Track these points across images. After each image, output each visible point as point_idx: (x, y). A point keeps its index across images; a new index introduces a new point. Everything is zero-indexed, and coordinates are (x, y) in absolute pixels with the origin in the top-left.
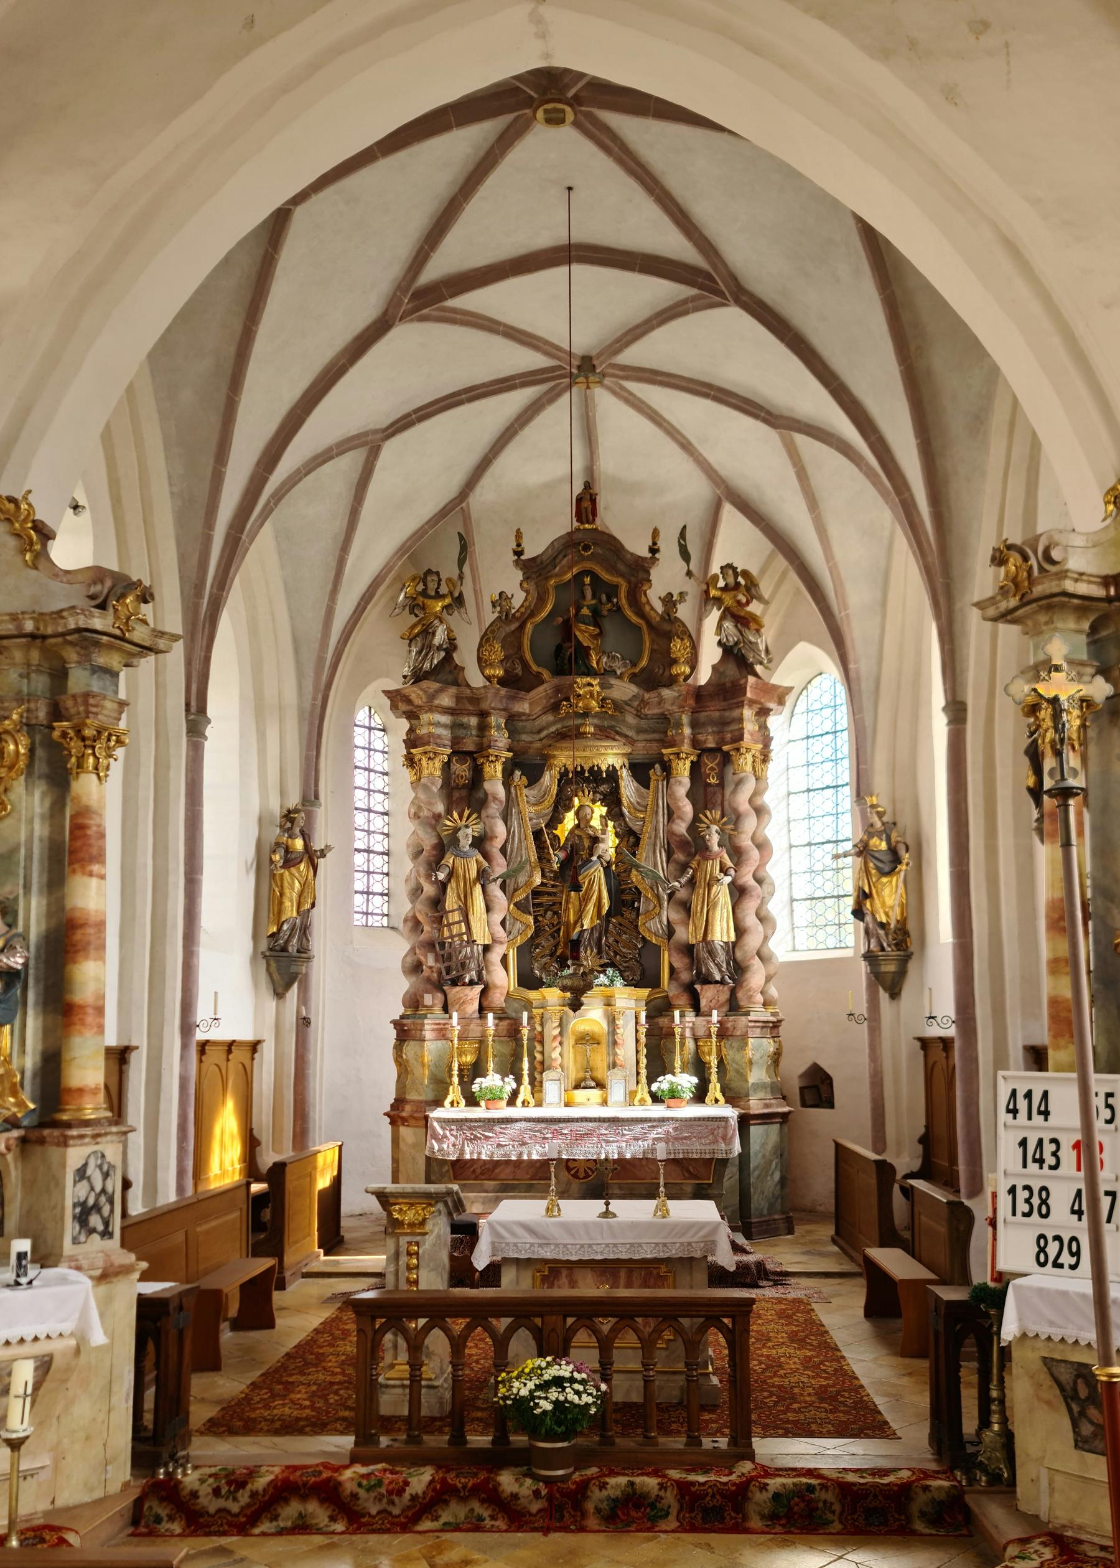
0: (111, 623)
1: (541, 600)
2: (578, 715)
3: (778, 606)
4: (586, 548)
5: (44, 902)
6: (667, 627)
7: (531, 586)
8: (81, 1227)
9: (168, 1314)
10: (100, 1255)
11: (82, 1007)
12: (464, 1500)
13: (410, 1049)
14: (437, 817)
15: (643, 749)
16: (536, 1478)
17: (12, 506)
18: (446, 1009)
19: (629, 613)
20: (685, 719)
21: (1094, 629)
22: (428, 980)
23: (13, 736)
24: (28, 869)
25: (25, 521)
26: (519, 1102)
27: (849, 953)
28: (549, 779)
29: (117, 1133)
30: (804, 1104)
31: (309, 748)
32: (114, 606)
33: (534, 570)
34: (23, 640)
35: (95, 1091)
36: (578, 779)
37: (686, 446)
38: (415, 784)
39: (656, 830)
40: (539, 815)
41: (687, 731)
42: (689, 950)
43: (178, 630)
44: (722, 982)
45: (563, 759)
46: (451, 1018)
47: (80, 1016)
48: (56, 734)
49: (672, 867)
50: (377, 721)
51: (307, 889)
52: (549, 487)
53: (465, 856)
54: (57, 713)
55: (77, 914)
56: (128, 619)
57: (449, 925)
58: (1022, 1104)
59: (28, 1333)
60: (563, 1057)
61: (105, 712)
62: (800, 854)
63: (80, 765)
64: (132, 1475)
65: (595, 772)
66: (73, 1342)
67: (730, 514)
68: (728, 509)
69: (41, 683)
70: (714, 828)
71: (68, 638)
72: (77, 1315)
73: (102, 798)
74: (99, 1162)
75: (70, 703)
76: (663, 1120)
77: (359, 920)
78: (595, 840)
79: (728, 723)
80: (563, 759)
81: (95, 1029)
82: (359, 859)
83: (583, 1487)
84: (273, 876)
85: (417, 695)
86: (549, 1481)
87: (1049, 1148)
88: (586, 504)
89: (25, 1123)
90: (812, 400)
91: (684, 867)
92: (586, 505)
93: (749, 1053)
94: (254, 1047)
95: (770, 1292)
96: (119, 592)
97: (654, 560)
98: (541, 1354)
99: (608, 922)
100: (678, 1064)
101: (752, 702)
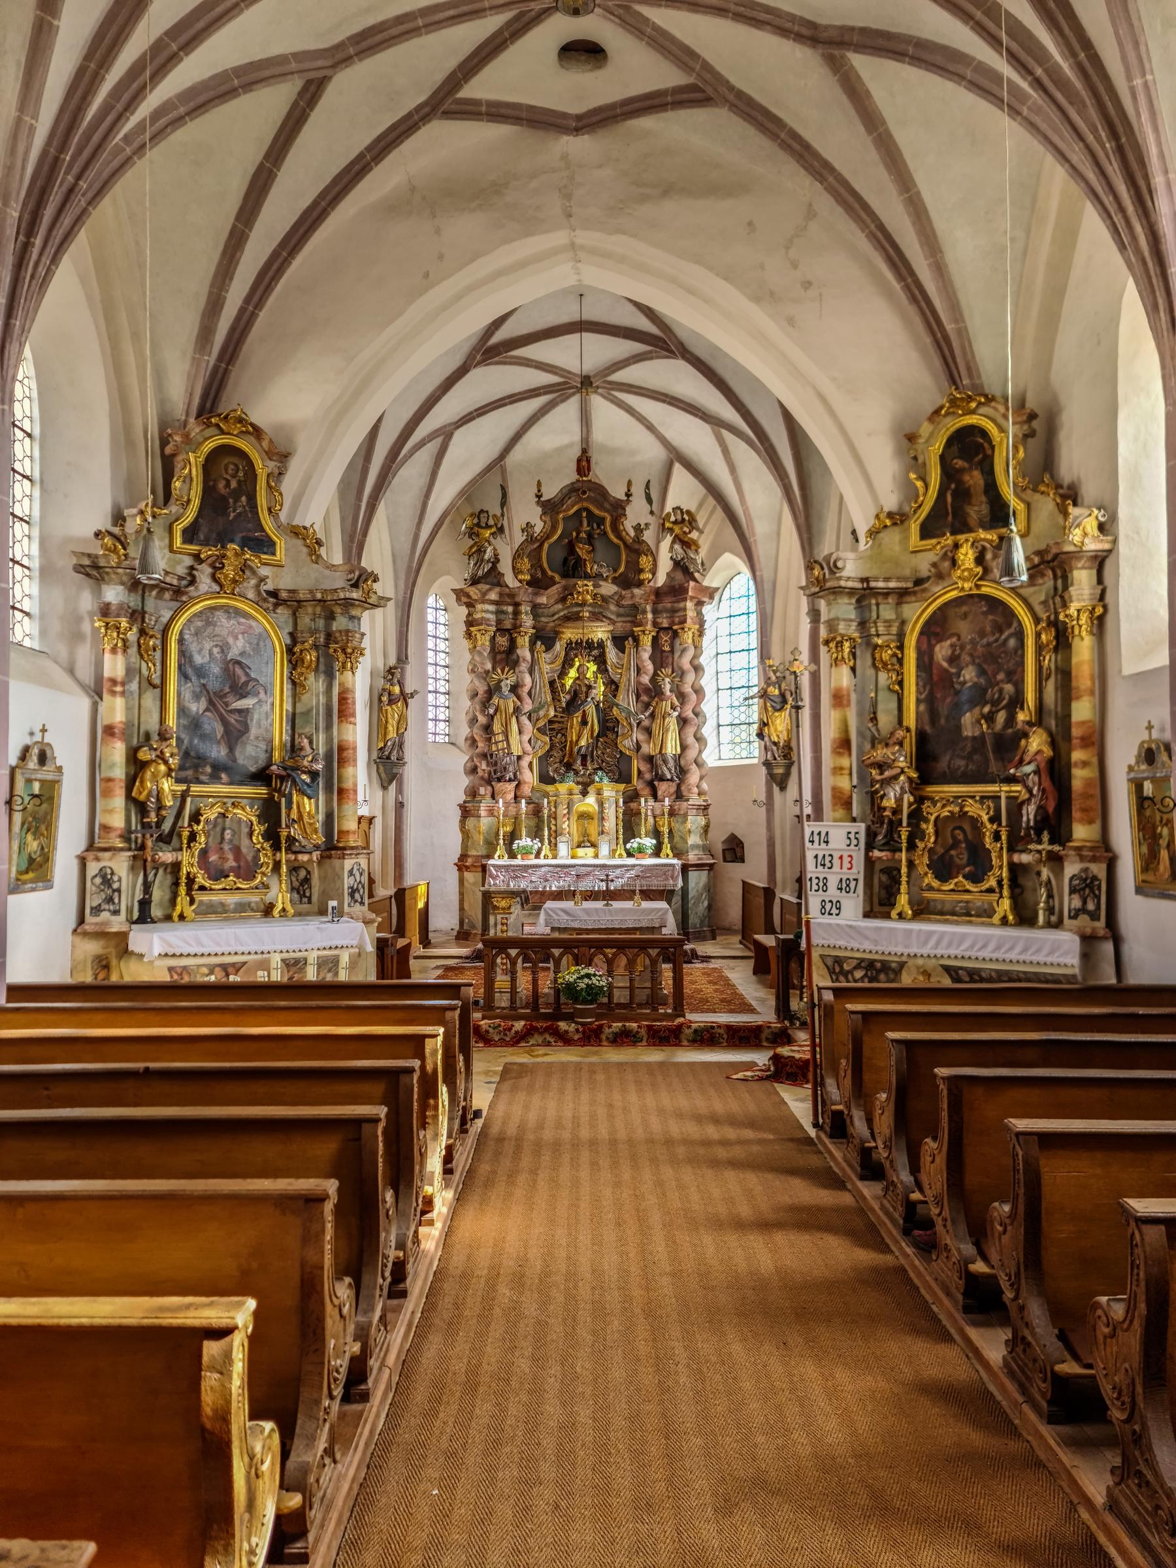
1: (554, 528)
2: (577, 605)
3: (711, 529)
4: (584, 493)
6: (637, 546)
7: (548, 519)
12: (541, 1033)
13: (470, 822)
14: (487, 672)
15: (621, 627)
16: (577, 1023)
18: (493, 797)
19: (612, 537)
20: (649, 608)
21: (858, 601)
22: (482, 778)
26: (542, 855)
27: (755, 761)
28: (559, 647)
30: (725, 860)
31: (401, 626)
33: (549, 508)
36: (574, 648)
37: (650, 428)
38: (473, 650)
39: (629, 680)
40: (553, 671)
41: (650, 616)
42: (650, 759)
43: (392, 596)
44: (672, 780)
45: (570, 634)
46: (497, 802)
48: (331, 650)
49: (639, 705)
50: (441, 603)
51: (402, 719)
52: (559, 450)
53: (506, 698)
57: (496, 743)
58: (816, 838)
60: (569, 826)
62: (724, 695)
65: (590, 645)
67: (678, 470)
68: (677, 467)
69: (321, 623)
70: (667, 680)
76: (634, 866)
77: (431, 738)
78: (589, 687)
79: (677, 611)
80: (570, 634)
82: (431, 697)
83: (601, 1027)
84: (380, 709)
85: (474, 592)
86: (583, 1024)
87: (828, 859)
88: (584, 463)
90: (729, 413)
91: (647, 706)
92: (584, 464)
93: (689, 825)
94: (371, 820)
95: (698, 965)
97: (628, 501)
98: (577, 965)
99: (598, 741)
100: (643, 831)
101: (692, 598)
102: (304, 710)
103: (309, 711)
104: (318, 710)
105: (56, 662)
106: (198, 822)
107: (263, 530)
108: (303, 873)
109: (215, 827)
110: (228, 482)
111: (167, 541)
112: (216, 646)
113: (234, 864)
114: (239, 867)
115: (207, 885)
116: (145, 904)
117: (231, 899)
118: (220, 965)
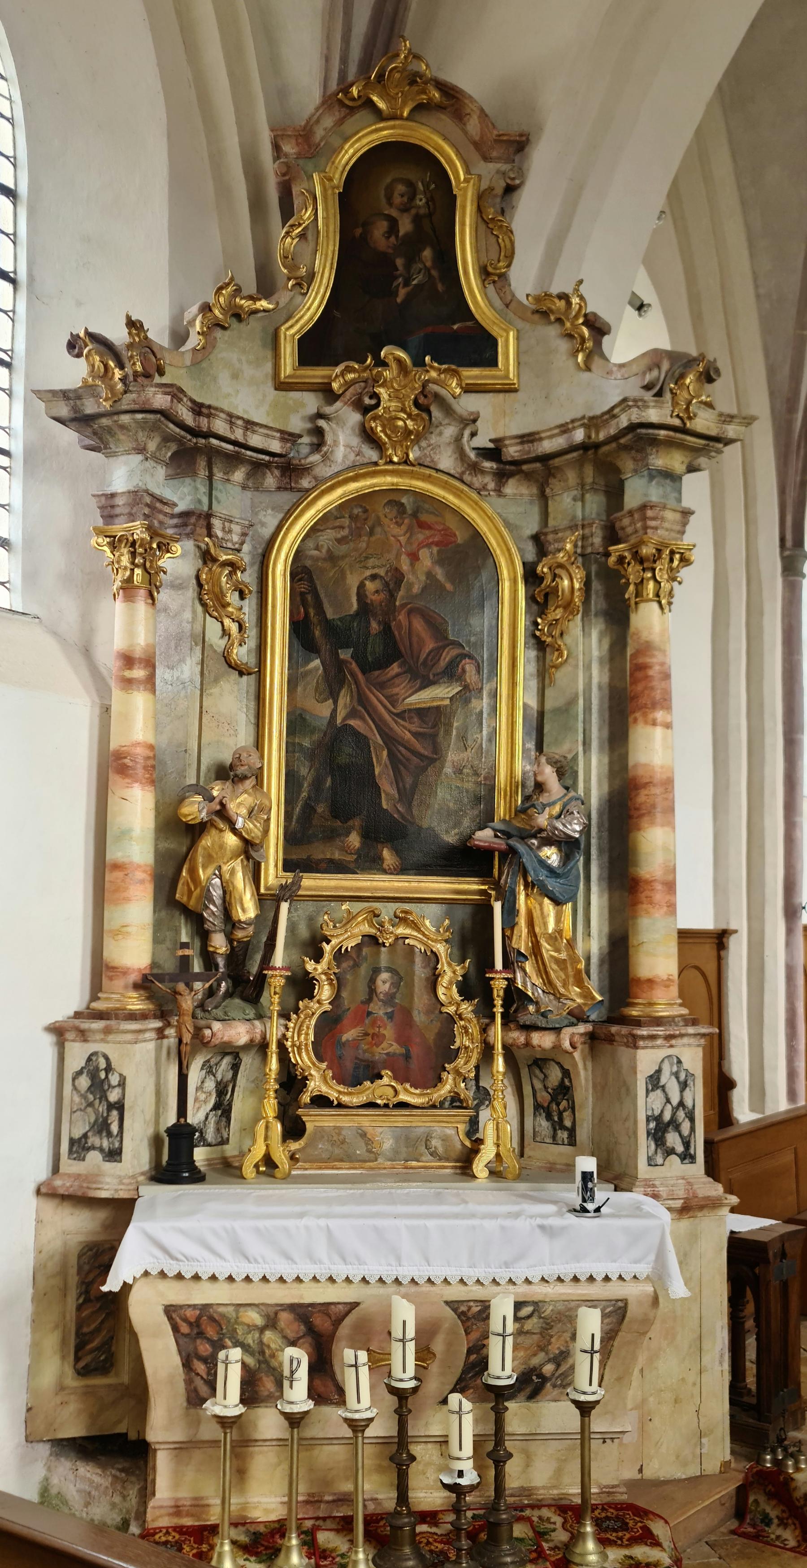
0: (669, 413)
5: (606, 760)
8: (657, 1146)
9: (767, 1261)
10: (681, 1181)
11: (649, 882)
17: (561, 304)
23: (568, 571)
24: (587, 722)
25: (576, 317)
29: (695, 1035)
32: (671, 390)
34: (575, 454)
35: (667, 984)
48: (612, 560)
54: (612, 536)
55: (640, 772)
56: (689, 403)
59: (599, 1270)
61: (666, 525)
63: (638, 594)
64: (733, 1452)
66: (650, 1289)
69: (595, 504)
71: (622, 441)
72: (652, 1257)
73: (664, 630)
74: (675, 1069)
75: (626, 521)
81: (665, 909)
89: (593, 1017)
96: (677, 374)
102: (561, 702)
105: (55, 634)
106: (318, 956)
107: (471, 317)
108: (555, 1075)
109: (356, 965)
110: (393, 224)
111: (269, 367)
112: (374, 577)
113: (395, 1048)
114: (407, 1056)
115: (333, 1095)
117: (384, 1130)
118: (293, 1308)
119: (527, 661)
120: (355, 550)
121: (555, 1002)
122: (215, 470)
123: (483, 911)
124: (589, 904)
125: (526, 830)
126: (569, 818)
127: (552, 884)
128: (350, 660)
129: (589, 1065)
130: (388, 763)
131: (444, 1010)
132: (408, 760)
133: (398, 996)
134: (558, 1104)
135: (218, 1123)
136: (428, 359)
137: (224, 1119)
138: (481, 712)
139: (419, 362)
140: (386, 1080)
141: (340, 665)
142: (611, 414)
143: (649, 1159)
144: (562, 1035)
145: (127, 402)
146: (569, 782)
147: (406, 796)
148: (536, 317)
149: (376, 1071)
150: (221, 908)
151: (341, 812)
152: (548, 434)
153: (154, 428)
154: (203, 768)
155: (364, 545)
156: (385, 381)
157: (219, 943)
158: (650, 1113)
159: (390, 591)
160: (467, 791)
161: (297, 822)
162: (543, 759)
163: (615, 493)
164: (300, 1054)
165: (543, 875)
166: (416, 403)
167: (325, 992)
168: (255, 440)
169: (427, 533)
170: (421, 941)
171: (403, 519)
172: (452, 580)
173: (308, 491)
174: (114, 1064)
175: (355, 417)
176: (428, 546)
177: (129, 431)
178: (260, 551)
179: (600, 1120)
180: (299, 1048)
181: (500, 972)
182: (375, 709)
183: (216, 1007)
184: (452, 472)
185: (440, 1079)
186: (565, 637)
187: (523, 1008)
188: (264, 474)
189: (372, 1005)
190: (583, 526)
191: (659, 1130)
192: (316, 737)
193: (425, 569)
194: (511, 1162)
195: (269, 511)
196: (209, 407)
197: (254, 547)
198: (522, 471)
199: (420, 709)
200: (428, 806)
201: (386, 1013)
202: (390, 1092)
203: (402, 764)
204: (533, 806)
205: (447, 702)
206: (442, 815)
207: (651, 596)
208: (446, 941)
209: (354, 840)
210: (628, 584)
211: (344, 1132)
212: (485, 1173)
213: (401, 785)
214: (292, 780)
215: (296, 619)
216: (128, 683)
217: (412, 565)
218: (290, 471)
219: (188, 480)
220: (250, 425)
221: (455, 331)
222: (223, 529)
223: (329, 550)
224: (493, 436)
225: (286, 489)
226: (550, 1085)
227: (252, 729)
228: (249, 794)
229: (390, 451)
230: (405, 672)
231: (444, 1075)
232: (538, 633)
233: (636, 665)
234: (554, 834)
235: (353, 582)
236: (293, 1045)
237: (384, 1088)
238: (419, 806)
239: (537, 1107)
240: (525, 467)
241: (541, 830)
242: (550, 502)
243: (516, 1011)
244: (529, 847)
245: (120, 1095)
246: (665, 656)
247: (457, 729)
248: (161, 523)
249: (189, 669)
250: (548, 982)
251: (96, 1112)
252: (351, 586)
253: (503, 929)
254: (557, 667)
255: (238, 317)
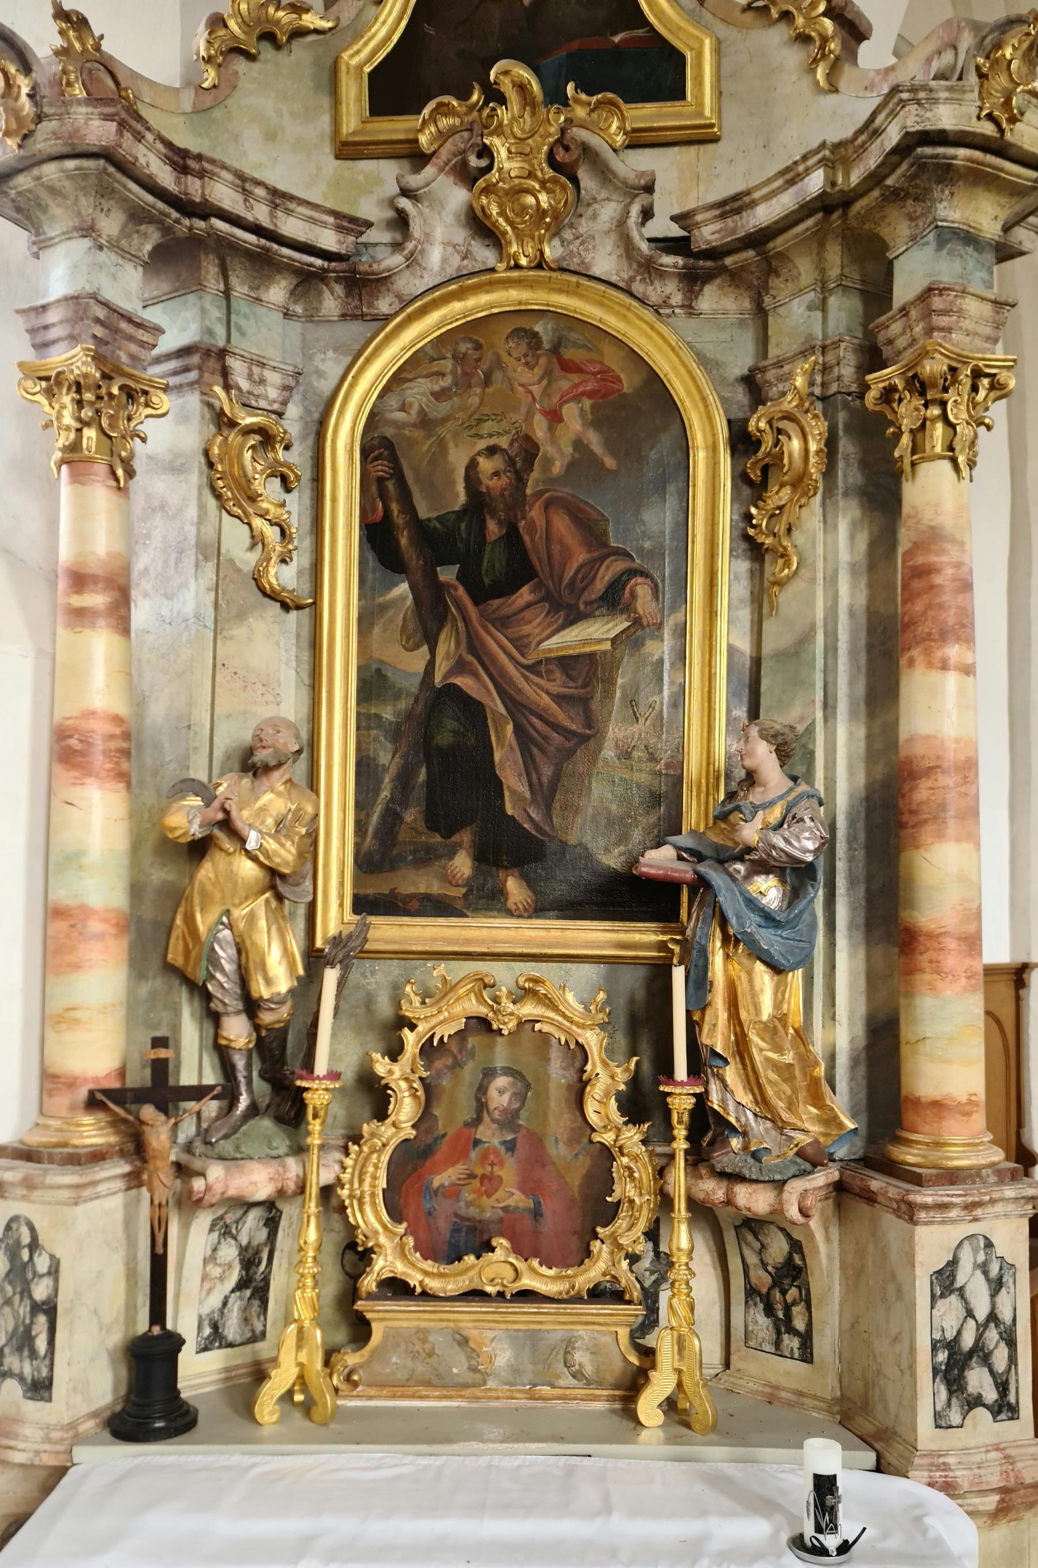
0: (974, 111)
5: (861, 732)
8: (951, 1392)
10: (994, 1455)
24: (830, 670)
34: (810, 222)
35: (965, 1110)
47: (931, 954)
48: (872, 395)
54: (873, 358)
55: (919, 749)
61: (966, 324)
69: (843, 312)
74: (981, 1258)
81: (963, 981)
89: (841, 1153)
103: (806, 639)
104: (831, 636)
106: (394, 1052)
107: (644, 22)
108: (778, 1248)
111: (325, 121)
112: (492, 451)
113: (518, 1199)
114: (537, 1213)
115: (414, 1279)
116: (151, 1359)
117: (497, 1340)
119: (735, 578)
120: (463, 408)
121: (773, 1133)
122: (234, 281)
123: (659, 976)
124: (833, 967)
125: (726, 848)
126: (795, 828)
127: (768, 939)
128: (456, 583)
129: (835, 1232)
130: (514, 743)
131: (596, 1138)
132: (545, 738)
133: (523, 1114)
134: (784, 1293)
135: (245, 1310)
136: (570, 88)
137: (256, 1303)
138: (661, 661)
139: (556, 97)
140: (499, 1254)
141: (439, 590)
142: (870, 129)
143: (937, 1416)
144: (785, 1195)
145: (43, 142)
146: (800, 770)
147: (546, 795)
148: (749, 16)
149: (486, 1237)
150: (235, 977)
151: (443, 820)
152: (765, 190)
153: (104, 191)
154: (218, 753)
155: (475, 400)
156: (500, 124)
157: (237, 1031)
158: (937, 1336)
159: (517, 473)
160: (638, 786)
161: (375, 835)
162: (754, 731)
163: (876, 295)
164: (361, 1210)
165: (752, 924)
166: (551, 160)
167: (405, 1109)
168: (292, 227)
169: (576, 378)
170: (560, 1027)
171: (538, 357)
172: (613, 452)
173: (387, 319)
174: (42, 1239)
175: (457, 196)
176: (577, 398)
177: (65, 197)
178: (316, 416)
179: (853, 1326)
180: (361, 1204)
181: (682, 1084)
182: (494, 660)
183: (226, 1137)
184: (614, 279)
185: (588, 1253)
186: (795, 533)
187: (720, 1141)
188: (320, 294)
189: (481, 1128)
190: (824, 349)
191: (954, 1364)
192: (403, 705)
193: (572, 436)
194: (702, 1404)
195: (330, 354)
196: (199, 157)
197: (307, 411)
198: (724, 269)
199: (564, 657)
200: (577, 811)
201: (504, 1143)
202: (510, 1273)
203: (537, 745)
204: (738, 808)
205: (607, 646)
206: (598, 826)
207: (938, 449)
208: (602, 1026)
209: (462, 864)
210: (898, 435)
211: (432, 1338)
212: (659, 1418)
213: (534, 777)
214: (366, 770)
215: (371, 519)
216: (80, 616)
217: (551, 429)
218: (360, 284)
219: (192, 298)
220: (278, 198)
221: (617, 46)
222: (250, 376)
223: (422, 411)
224: (677, 211)
225: (354, 317)
226: (770, 1261)
227: (305, 693)
228: (279, 794)
229: (514, 248)
230: (539, 601)
231: (596, 1246)
232: (751, 532)
233: (912, 568)
234: (769, 855)
235: (458, 458)
236: (351, 1196)
237: (497, 1268)
238: (565, 807)
239: (751, 1292)
240: (728, 261)
241: (749, 850)
242: (770, 318)
243: (711, 1144)
244: (731, 876)
245: (50, 1291)
246: (963, 551)
247: (622, 687)
248: (133, 357)
249: (193, 595)
250: (762, 1100)
251: (16, 1315)
252: (458, 464)
253: (688, 1012)
254: (780, 583)
255: (269, 37)
